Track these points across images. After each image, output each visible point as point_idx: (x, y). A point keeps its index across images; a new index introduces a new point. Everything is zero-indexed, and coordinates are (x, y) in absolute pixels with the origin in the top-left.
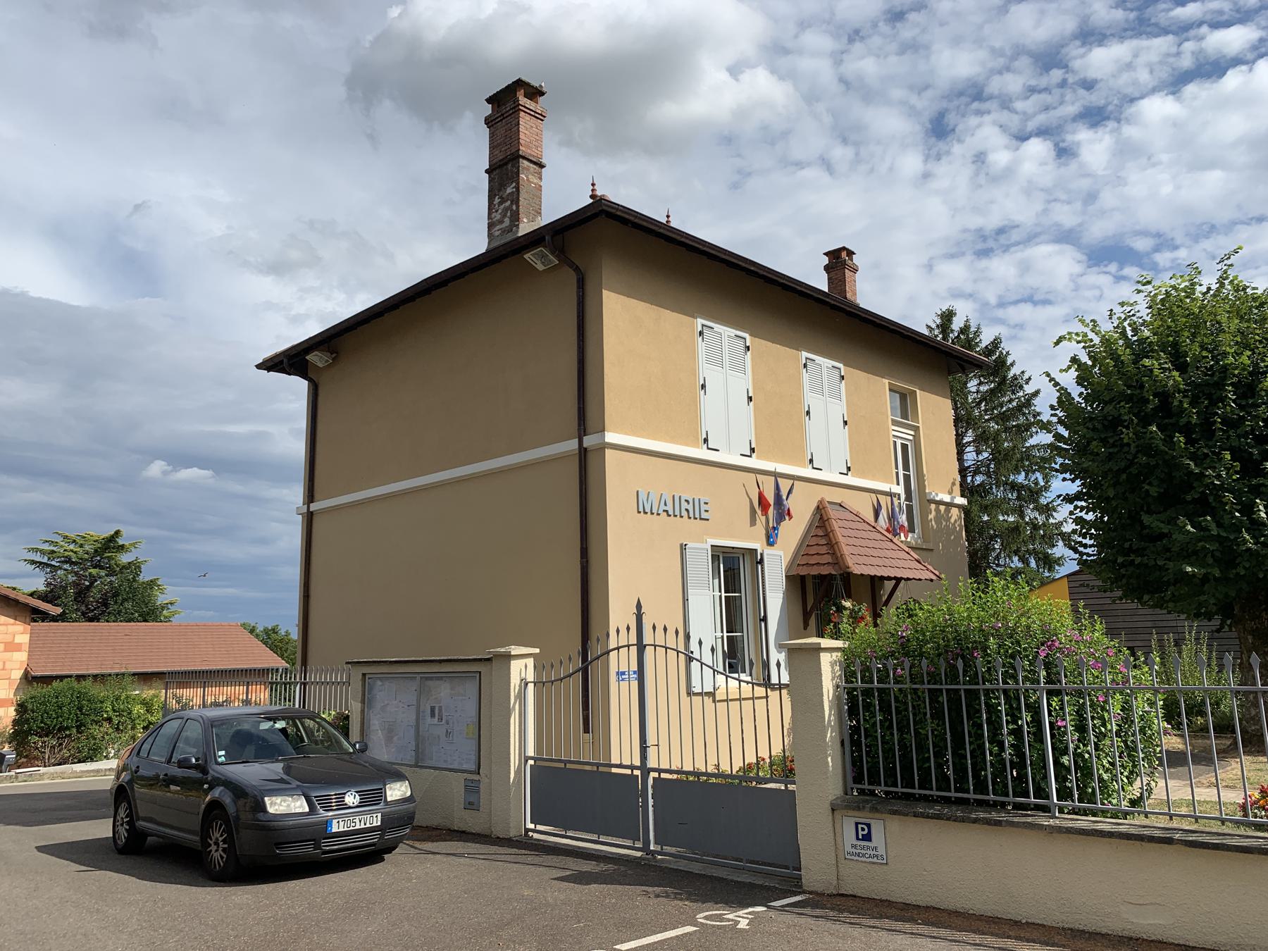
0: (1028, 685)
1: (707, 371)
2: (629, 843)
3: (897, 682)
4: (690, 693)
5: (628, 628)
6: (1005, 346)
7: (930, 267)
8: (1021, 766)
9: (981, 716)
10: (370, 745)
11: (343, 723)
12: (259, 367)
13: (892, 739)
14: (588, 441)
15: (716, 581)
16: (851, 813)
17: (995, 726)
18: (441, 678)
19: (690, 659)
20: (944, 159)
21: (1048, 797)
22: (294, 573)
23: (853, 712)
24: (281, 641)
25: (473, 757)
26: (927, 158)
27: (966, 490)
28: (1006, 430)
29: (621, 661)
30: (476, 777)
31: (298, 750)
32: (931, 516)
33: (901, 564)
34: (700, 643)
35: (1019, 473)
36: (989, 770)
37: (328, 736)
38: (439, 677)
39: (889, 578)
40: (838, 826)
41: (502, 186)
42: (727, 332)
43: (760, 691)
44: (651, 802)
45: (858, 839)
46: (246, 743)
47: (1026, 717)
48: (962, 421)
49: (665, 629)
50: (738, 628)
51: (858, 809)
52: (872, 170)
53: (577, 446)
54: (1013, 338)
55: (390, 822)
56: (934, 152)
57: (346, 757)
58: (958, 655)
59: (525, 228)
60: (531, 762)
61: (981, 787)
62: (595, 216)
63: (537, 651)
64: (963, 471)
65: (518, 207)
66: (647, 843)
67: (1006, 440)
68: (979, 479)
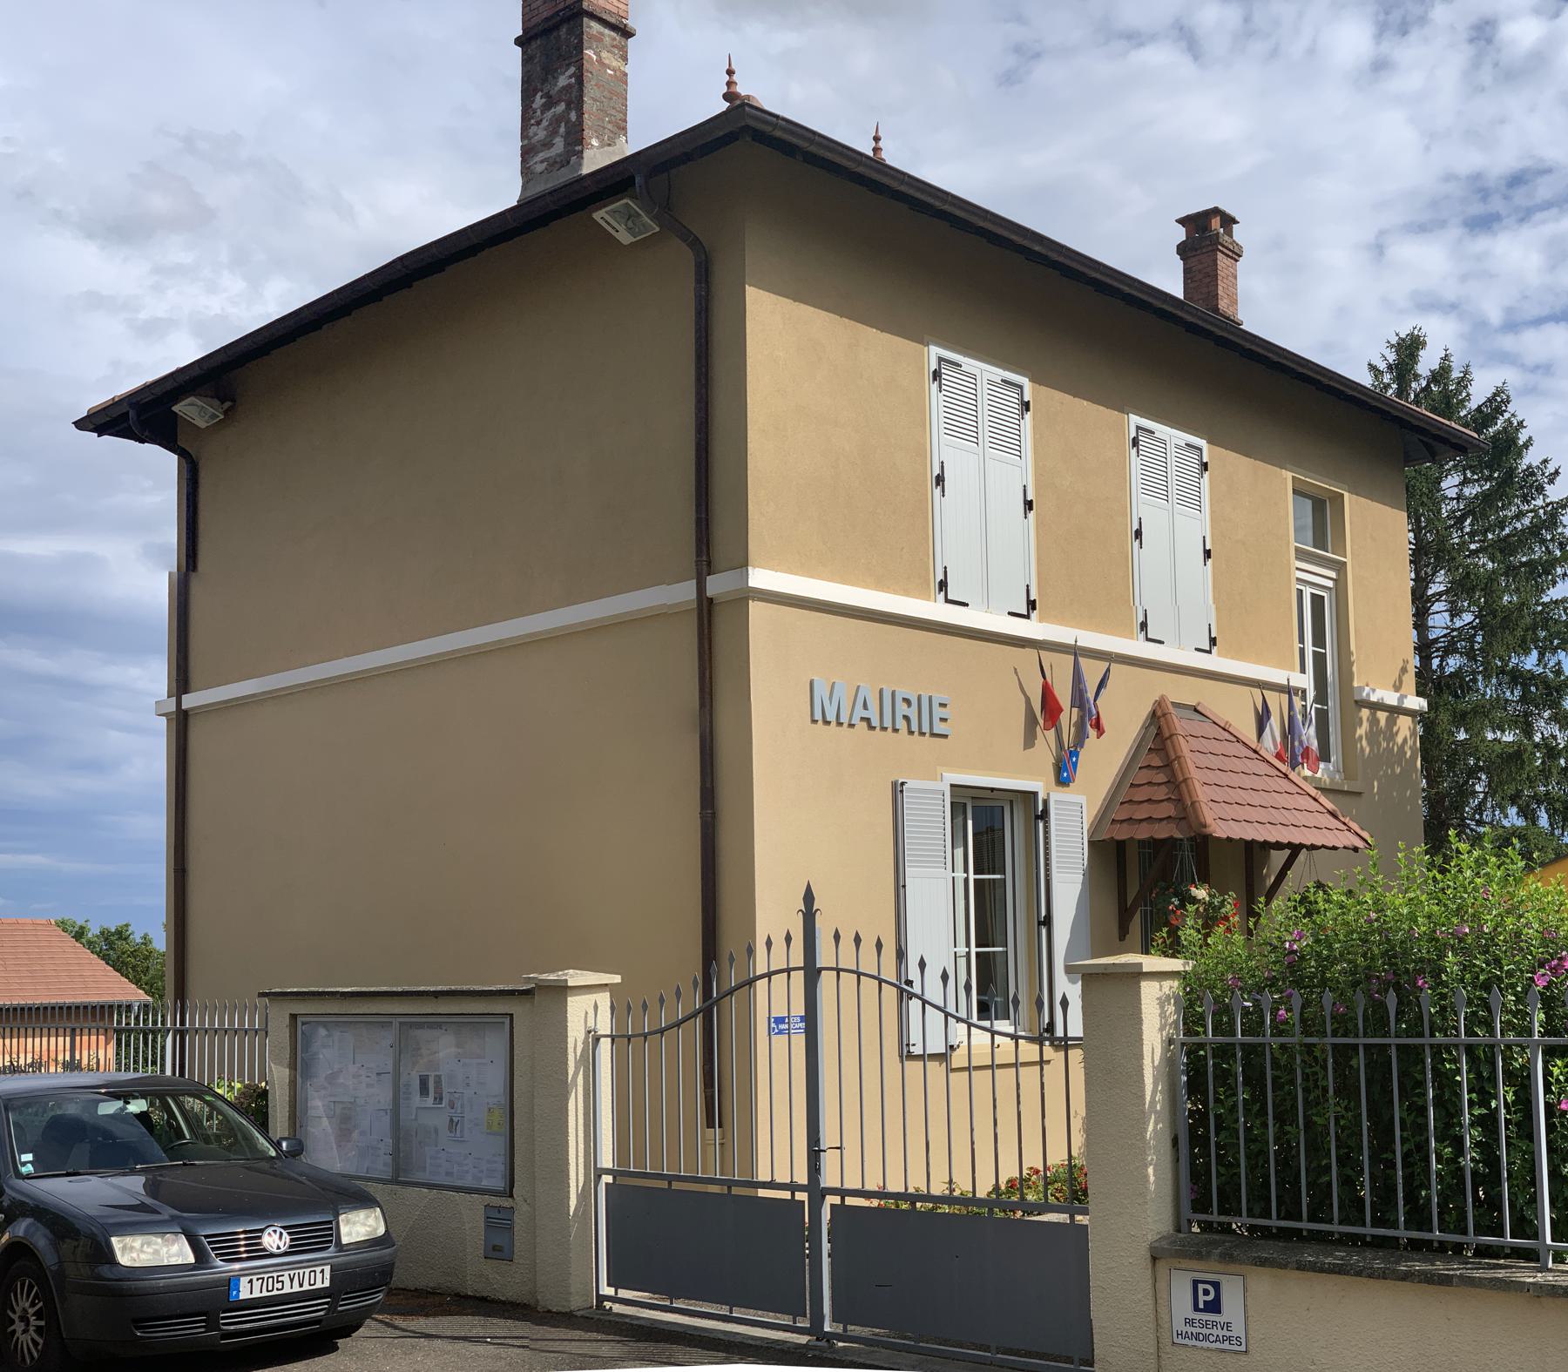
0: (1511, 1037)
1: (950, 451)
2: (785, 1320)
3: (1278, 1031)
4: (906, 1055)
5: (788, 939)
6: (1517, 408)
7: (1378, 249)
8: (1492, 1180)
9: (1425, 1094)
10: (309, 1144)
11: (256, 1104)
12: (80, 424)
13: (1265, 1134)
14: (716, 585)
15: (959, 852)
16: (1186, 1263)
17: (1448, 1110)
18: (439, 1026)
19: (905, 994)
20: (1415, 35)
21: (1536, 1234)
22: (155, 827)
23: (1196, 1086)
24: (133, 954)
25: (500, 1167)
26: (1382, 30)
27: (1427, 682)
28: (1511, 571)
29: (777, 998)
30: (506, 1203)
31: (173, 1153)
32: (1361, 731)
33: (1301, 818)
34: (922, 965)
35: (1527, 652)
36: (1435, 1187)
37: (229, 1127)
38: (435, 1022)
39: (1279, 846)
40: (1161, 1285)
41: (549, 73)
42: (987, 373)
43: (1029, 1051)
44: (826, 1247)
45: (1196, 1309)
46: (72, 1139)
47: (1505, 1093)
48: (1426, 555)
49: (858, 940)
50: (999, 938)
51: (1199, 1256)
52: (1274, 53)
53: (694, 596)
54: (1531, 391)
55: (349, 1280)
56: (1396, 16)
57: (264, 1165)
58: (1387, 983)
59: (596, 158)
60: (608, 1179)
61: (1419, 1218)
62: (730, 138)
63: (617, 979)
64: (1424, 648)
65: (580, 115)
66: (818, 1318)
67: (1507, 589)
68: (1453, 663)
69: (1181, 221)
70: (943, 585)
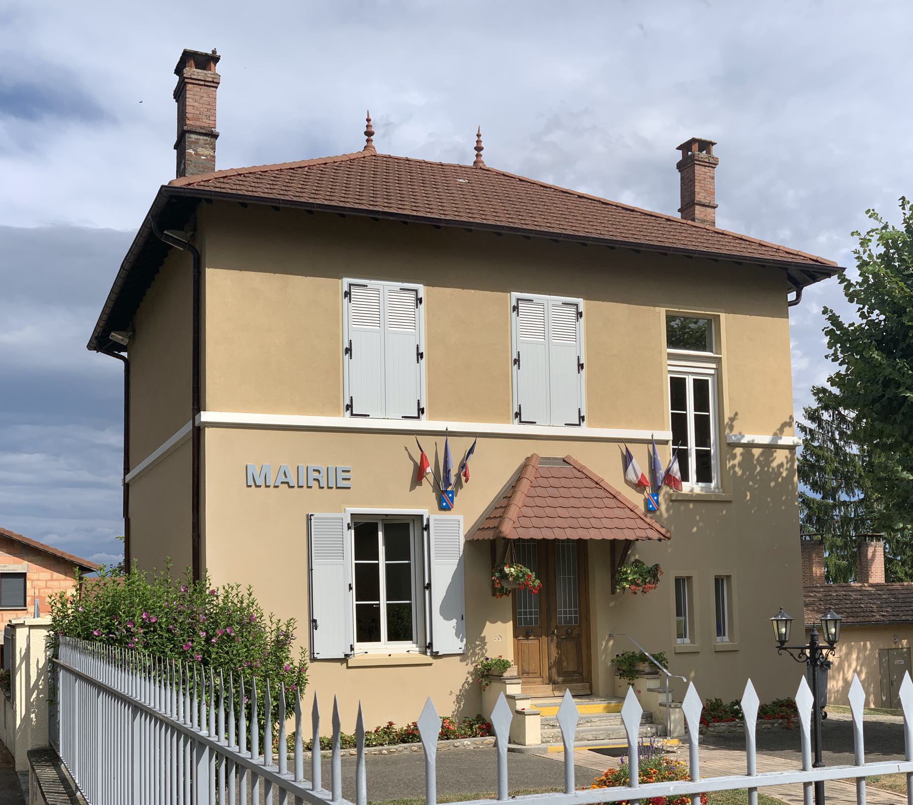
69: (678, 148)
70: (518, 415)
